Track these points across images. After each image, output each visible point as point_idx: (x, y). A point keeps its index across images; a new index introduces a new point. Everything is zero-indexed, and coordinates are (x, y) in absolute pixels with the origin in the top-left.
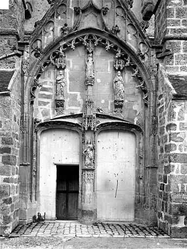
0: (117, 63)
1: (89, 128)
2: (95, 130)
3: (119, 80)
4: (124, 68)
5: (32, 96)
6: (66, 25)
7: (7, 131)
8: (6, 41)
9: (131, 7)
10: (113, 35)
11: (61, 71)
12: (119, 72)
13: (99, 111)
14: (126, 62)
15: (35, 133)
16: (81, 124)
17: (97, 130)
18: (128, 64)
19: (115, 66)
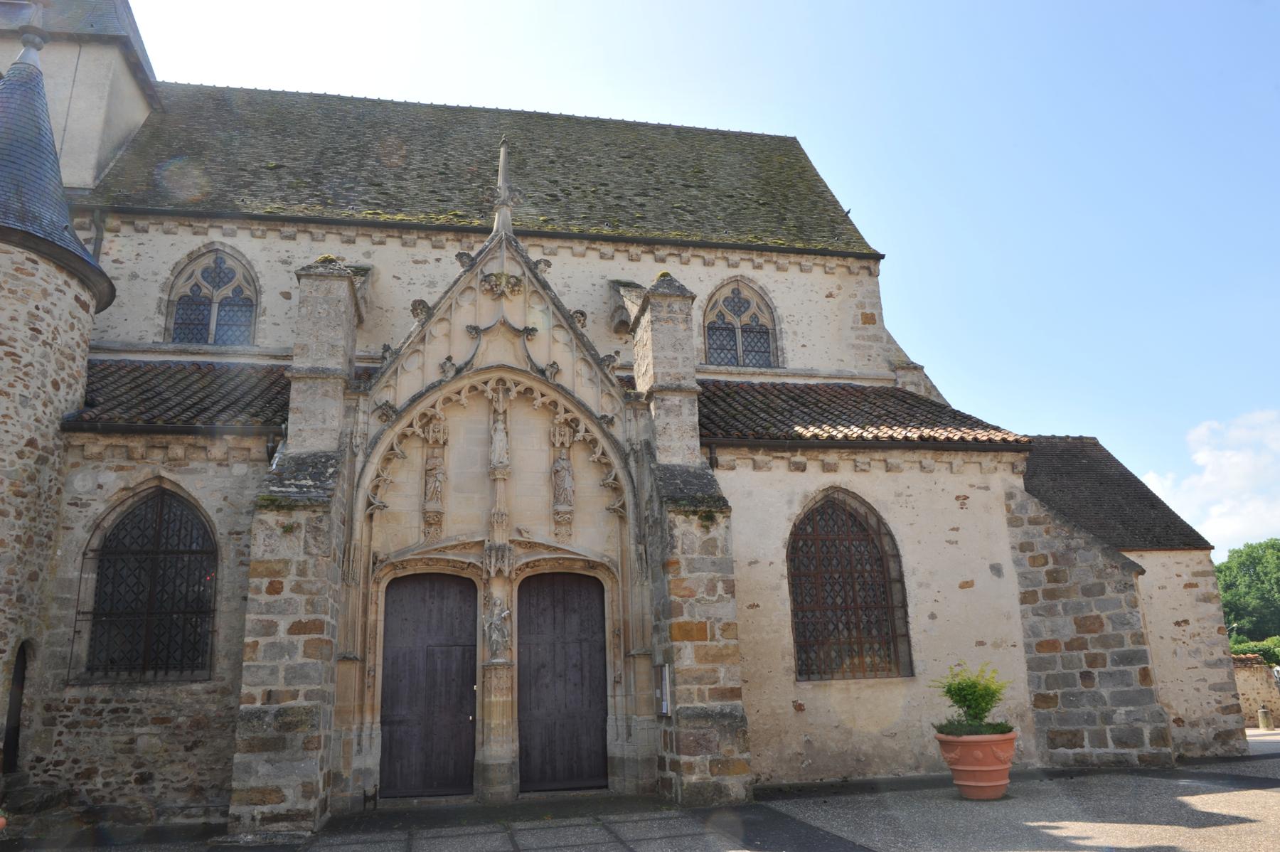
1: (499, 572)
2: (514, 576)
6: (449, 359)
7: (319, 585)
14: (576, 431)
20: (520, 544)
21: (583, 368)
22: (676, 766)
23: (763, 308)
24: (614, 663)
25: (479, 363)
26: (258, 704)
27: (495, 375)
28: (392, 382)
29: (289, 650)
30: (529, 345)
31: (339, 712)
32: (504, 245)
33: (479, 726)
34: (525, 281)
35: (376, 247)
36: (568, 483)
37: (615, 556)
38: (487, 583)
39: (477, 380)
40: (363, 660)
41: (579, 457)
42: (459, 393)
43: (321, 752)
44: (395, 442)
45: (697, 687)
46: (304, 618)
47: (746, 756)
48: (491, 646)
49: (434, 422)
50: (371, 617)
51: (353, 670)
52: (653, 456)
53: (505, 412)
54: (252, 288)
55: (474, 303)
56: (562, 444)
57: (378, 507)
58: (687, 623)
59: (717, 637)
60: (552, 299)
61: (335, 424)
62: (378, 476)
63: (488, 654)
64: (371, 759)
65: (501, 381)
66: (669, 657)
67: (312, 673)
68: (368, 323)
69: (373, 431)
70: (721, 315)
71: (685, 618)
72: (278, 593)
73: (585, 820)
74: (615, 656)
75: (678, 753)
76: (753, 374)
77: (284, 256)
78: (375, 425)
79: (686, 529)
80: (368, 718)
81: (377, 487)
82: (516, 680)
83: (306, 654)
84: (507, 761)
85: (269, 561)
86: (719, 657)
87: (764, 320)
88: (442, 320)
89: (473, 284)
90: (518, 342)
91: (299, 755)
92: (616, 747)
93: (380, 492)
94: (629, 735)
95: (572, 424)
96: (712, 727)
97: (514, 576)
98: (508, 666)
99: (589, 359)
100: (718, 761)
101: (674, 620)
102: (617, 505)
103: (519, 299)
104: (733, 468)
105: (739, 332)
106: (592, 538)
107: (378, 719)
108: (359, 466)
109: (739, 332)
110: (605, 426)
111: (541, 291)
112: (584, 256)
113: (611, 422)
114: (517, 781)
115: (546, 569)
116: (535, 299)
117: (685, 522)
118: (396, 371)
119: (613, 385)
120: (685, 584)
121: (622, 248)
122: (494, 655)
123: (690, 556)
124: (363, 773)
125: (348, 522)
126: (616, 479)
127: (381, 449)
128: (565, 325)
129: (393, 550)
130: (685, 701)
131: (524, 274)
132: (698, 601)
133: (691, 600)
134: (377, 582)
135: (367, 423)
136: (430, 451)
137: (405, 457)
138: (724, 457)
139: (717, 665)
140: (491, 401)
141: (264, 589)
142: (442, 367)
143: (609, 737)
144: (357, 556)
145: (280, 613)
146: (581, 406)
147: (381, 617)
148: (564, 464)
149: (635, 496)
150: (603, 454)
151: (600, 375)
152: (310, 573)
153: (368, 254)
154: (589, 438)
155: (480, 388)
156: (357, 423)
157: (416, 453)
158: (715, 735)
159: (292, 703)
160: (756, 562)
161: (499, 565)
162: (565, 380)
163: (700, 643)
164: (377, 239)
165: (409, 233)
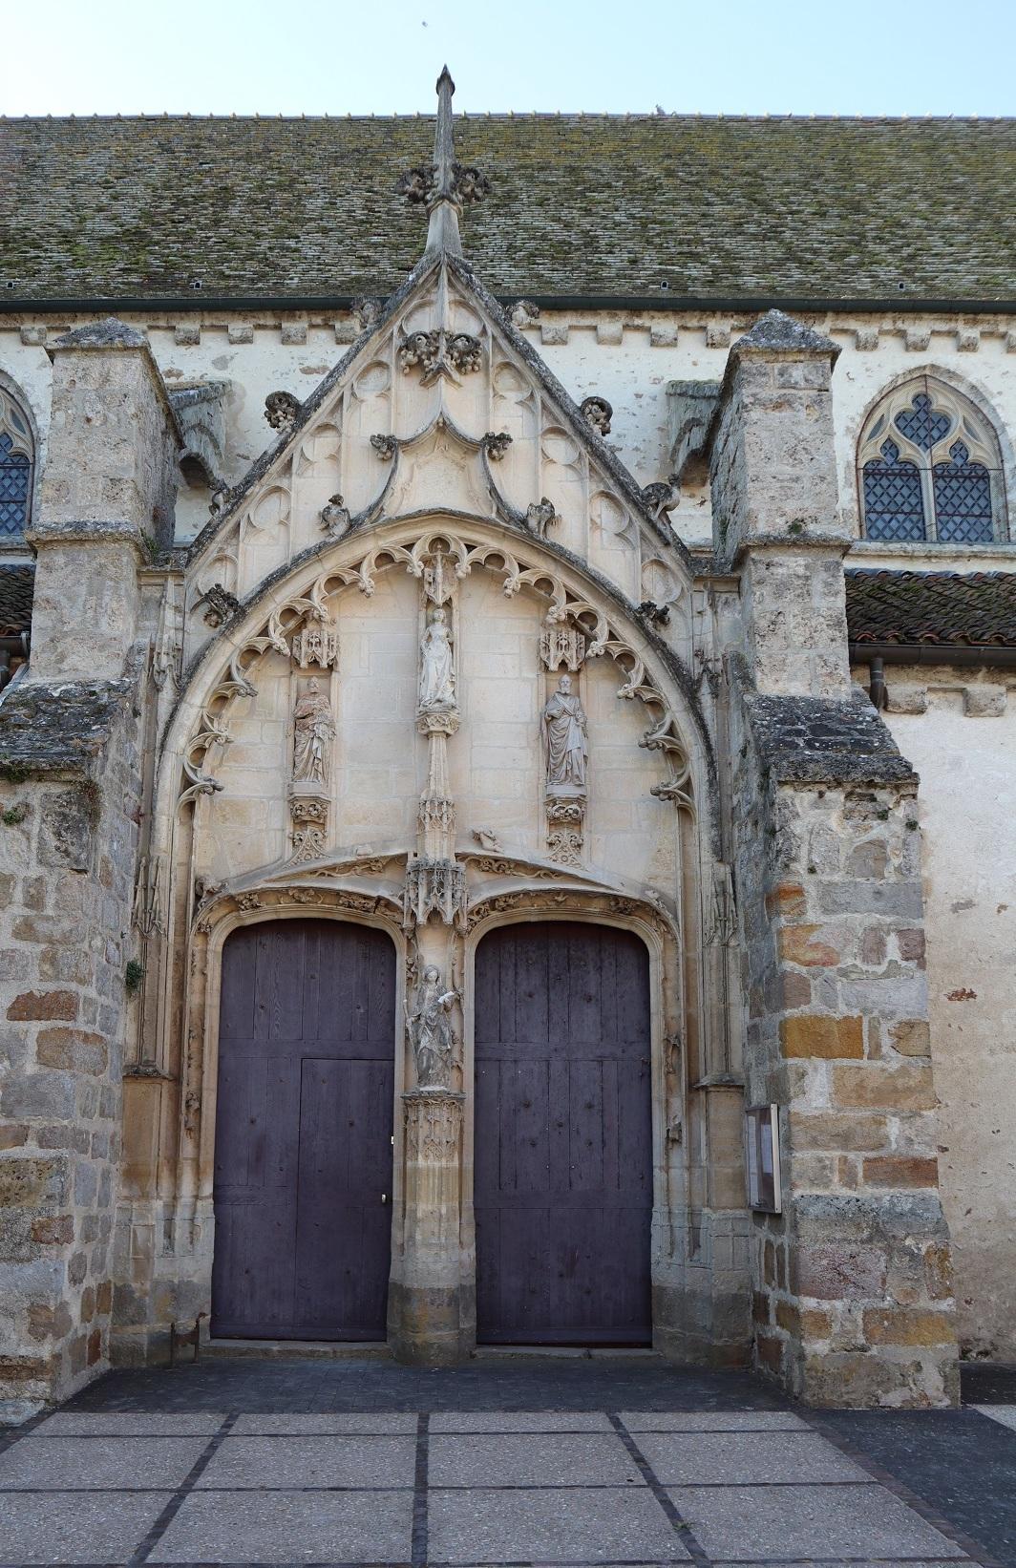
1: (435, 915)
2: (464, 924)
3: (565, 711)
5: (406, 1118)
7: (66, 924)
10: (532, 528)
14: (589, 639)
15: (199, 940)
16: (402, 898)
17: (473, 924)
20: (476, 861)
21: (604, 512)
22: (790, 1316)
23: (978, 428)
24: (667, 1109)
25: (395, 507)
27: (428, 532)
28: (229, 552)
30: (494, 469)
32: (444, 276)
33: (397, 1214)
34: (487, 345)
35: (236, 348)
36: (574, 740)
37: (672, 889)
38: (413, 936)
39: (391, 541)
40: (177, 1079)
41: (599, 692)
42: (357, 567)
44: (235, 662)
45: (838, 1153)
47: (946, 1305)
48: (419, 1059)
49: (311, 626)
50: (193, 1000)
52: (749, 682)
53: (448, 604)
54: (27, 437)
55: (385, 394)
56: (563, 664)
57: (202, 790)
59: (886, 1049)
60: (539, 376)
62: (203, 730)
63: (414, 1075)
64: (196, 1265)
65: (440, 541)
66: (779, 1090)
69: (193, 646)
70: (891, 447)
71: (815, 1006)
74: (669, 1089)
75: (795, 1292)
76: (958, 557)
78: (198, 631)
79: (817, 820)
81: (201, 751)
82: (470, 1129)
83: (42, 1059)
86: (889, 1094)
87: (979, 452)
88: (325, 427)
89: (384, 358)
90: (475, 463)
91: (24, 1251)
92: (668, 1271)
93: (209, 759)
94: (695, 1244)
95: (582, 623)
96: (870, 1240)
97: (464, 924)
98: (456, 1102)
99: (616, 493)
100: (884, 1314)
101: (788, 1012)
102: (674, 785)
103: (473, 383)
104: (920, 711)
105: (927, 480)
106: (628, 852)
107: (208, 1189)
109: (927, 480)
110: (649, 624)
111: (517, 362)
112: (618, 341)
114: (469, 1324)
116: (507, 380)
117: (815, 806)
120: (813, 938)
121: (694, 323)
122: (424, 1077)
123: (825, 878)
124: (177, 1293)
125: (144, 817)
128: (567, 427)
129: (233, 872)
130: (812, 1183)
131: (484, 332)
132: (844, 973)
133: (829, 972)
134: (205, 933)
135: (180, 626)
136: (304, 682)
137: (253, 694)
138: (901, 687)
140: (420, 581)
143: (654, 1248)
146: (597, 584)
148: (566, 703)
149: (711, 764)
150: (646, 682)
151: (639, 523)
152: (50, 900)
153: (222, 363)
154: (616, 651)
155: (397, 557)
156: (161, 628)
157: (275, 689)
160: (969, 904)
161: (433, 901)
162: (568, 536)
163: (846, 1062)
164: (236, 334)
165: (292, 317)
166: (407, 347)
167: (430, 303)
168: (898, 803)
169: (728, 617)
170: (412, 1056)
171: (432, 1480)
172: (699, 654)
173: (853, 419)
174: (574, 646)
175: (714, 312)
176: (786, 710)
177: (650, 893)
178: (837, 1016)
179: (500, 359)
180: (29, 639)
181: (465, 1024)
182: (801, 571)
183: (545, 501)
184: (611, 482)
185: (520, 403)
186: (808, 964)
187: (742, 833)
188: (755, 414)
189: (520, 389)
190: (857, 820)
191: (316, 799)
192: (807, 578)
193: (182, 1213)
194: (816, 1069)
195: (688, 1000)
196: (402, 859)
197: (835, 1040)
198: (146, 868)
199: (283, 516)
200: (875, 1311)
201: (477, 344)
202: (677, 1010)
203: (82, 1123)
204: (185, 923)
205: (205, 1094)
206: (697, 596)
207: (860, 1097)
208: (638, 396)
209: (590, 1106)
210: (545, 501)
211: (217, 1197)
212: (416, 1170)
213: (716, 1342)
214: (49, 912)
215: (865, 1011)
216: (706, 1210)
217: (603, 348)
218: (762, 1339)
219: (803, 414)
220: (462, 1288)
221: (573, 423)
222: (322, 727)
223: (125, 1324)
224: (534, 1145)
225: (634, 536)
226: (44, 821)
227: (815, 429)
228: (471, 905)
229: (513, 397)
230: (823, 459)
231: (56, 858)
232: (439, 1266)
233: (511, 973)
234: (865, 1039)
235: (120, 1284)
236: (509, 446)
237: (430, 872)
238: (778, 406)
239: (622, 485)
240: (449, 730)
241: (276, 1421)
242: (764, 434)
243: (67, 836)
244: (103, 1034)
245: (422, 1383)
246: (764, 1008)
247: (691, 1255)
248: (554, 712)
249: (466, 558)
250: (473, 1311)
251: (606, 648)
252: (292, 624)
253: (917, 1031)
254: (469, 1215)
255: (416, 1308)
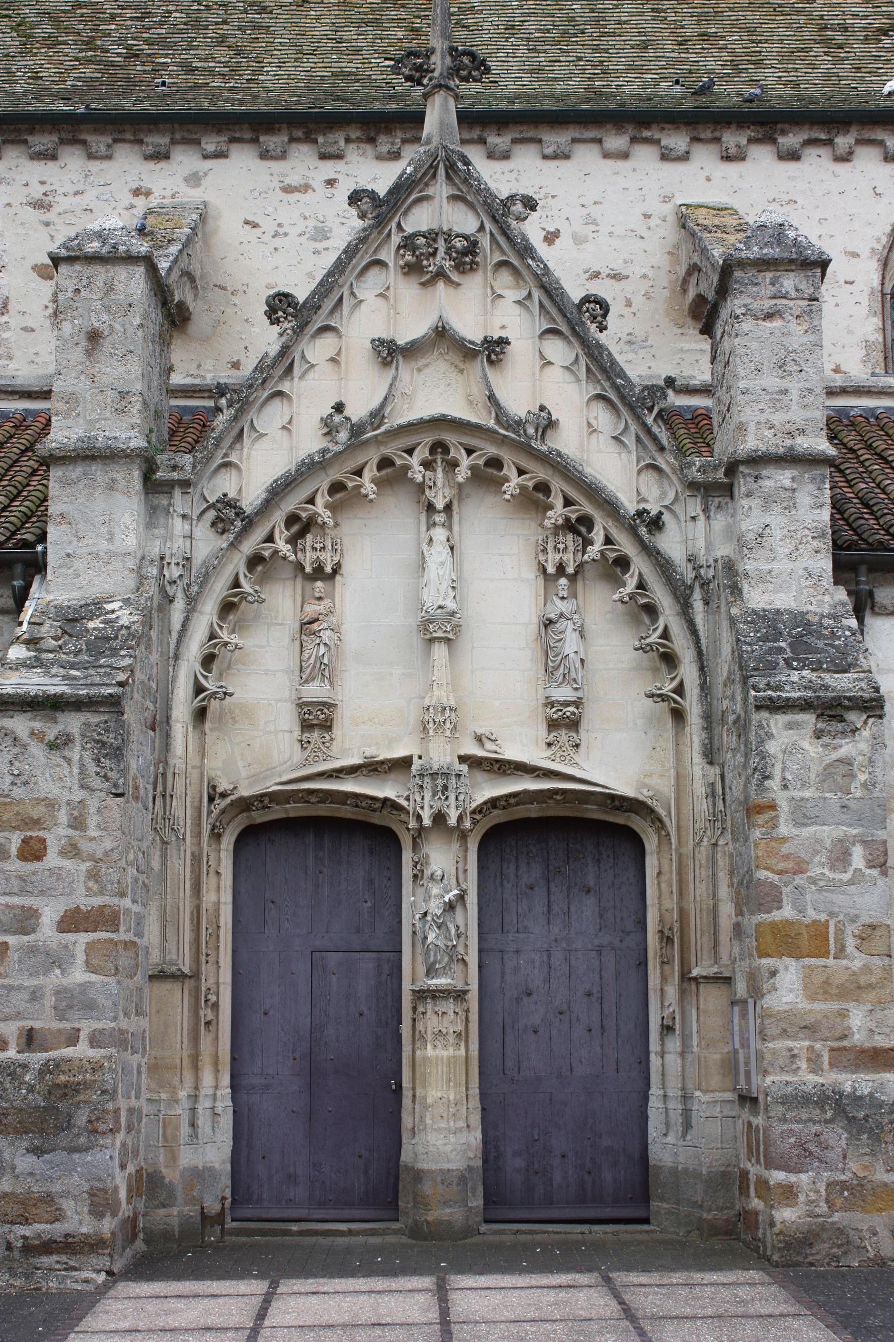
0: (550, 547)
1: (439, 818)
2: (467, 824)
3: (561, 615)
4: (580, 568)
6: (339, 408)
8: (178, 523)
9: (602, 328)
11: (319, 584)
12: (563, 581)
13: (482, 745)
16: (407, 799)
17: (475, 822)
18: (594, 550)
19: (542, 558)
21: (602, 416)
24: (663, 998)
26: (11, 1053)
28: (233, 458)
29: (58, 960)
31: (155, 1068)
32: (441, 171)
33: (406, 1101)
34: (485, 242)
35: (209, 164)
36: (571, 644)
40: (196, 975)
43: (120, 1137)
45: (807, 1043)
46: (86, 902)
50: (209, 898)
51: (176, 1000)
52: (736, 590)
53: (448, 508)
57: (214, 695)
58: (787, 923)
59: (850, 948)
61: (131, 542)
63: (422, 969)
64: (214, 1151)
67: (101, 1000)
68: (201, 320)
71: (787, 912)
72: (39, 858)
73: (583, 1279)
74: (664, 979)
77: (37, 192)
78: (206, 543)
80: (207, 1079)
82: (474, 1017)
84: (456, 1164)
85: (20, 801)
86: (853, 989)
88: (326, 329)
89: (383, 256)
92: (665, 1148)
94: (687, 1125)
96: (831, 1121)
98: (460, 995)
100: (843, 1185)
102: (668, 688)
106: (617, 759)
107: (226, 1080)
108: (176, 625)
110: (643, 531)
113: (656, 524)
114: (477, 1202)
115: (533, 811)
116: (505, 277)
118: (290, 369)
119: (662, 449)
120: (785, 849)
121: (708, 134)
122: (430, 972)
123: (798, 794)
124: (199, 1176)
125: (160, 724)
126: (665, 635)
127: (219, 589)
128: (564, 328)
131: (482, 228)
133: (799, 880)
139: (851, 1005)
141: (14, 851)
142: (329, 429)
144: (179, 789)
145: (42, 893)
147: (227, 897)
149: (702, 668)
150: (641, 585)
151: (633, 427)
152: (92, 821)
156: (169, 537)
158: (837, 1137)
159: (68, 1052)
161: (437, 805)
162: (567, 441)
163: (813, 961)
164: (211, 148)
166: (404, 247)
167: (427, 198)
168: (865, 722)
169: (719, 521)
170: (419, 949)
171: (453, 1318)
172: (691, 559)
173: (878, 240)
174: (571, 549)
175: (729, 124)
176: (769, 623)
177: (645, 791)
178: (807, 921)
179: (498, 257)
180: (45, 553)
181: (469, 918)
182: (787, 483)
183: (542, 408)
184: (607, 385)
185: (518, 302)
186: (780, 873)
187: (728, 739)
188: (747, 325)
189: (518, 286)
190: (826, 739)
191: (324, 704)
192: (794, 490)
193: (204, 1104)
194: (786, 969)
195: (681, 894)
196: (405, 763)
197: (804, 942)
198: (164, 775)
199: (286, 419)
200: (836, 1183)
201: (475, 244)
202: (671, 903)
203: (124, 1023)
204: (199, 825)
205: (221, 987)
206: (690, 501)
207: (825, 992)
208: (647, 216)
209: (589, 994)
210: (542, 408)
211: (234, 1087)
212: (425, 1058)
213: (705, 1215)
214: (93, 833)
215: (831, 914)
216: (698, 1093)
217: (609, 163)
218: (746, 1212)
219: (793, 326)
220: (470, 1168)
221: (569, 322)
222: (328, 632)
223: (157, 1207)
224: (535, 1032)
225: (630, 441)
226: (84, 749)
227: (805, 339)
228: (474, 805)
229: (512, 295)
230: (811, 371)
231: (97, 783)
232: (448, 1148)
233: (512, 867)
234: (832, 941)
235: (150, 1170)
236: (509, 349)
237: (434, 776)
238: (769, 316)
239: (617, 388)
240: (451, 636)
241: (310, 1284)
242: (754, 345)
243: (106, 762)
244: (136, 939)
245: (439, 1252)
246: (745, 909)
247: (684, 1136)
248: (552, 616)
249: (465, 462)
250: (480, 1190)
251: (602, 552)
252: (295, 528)
253: (878, 933)
254: (475, 1102)
255: (427, 1188)
